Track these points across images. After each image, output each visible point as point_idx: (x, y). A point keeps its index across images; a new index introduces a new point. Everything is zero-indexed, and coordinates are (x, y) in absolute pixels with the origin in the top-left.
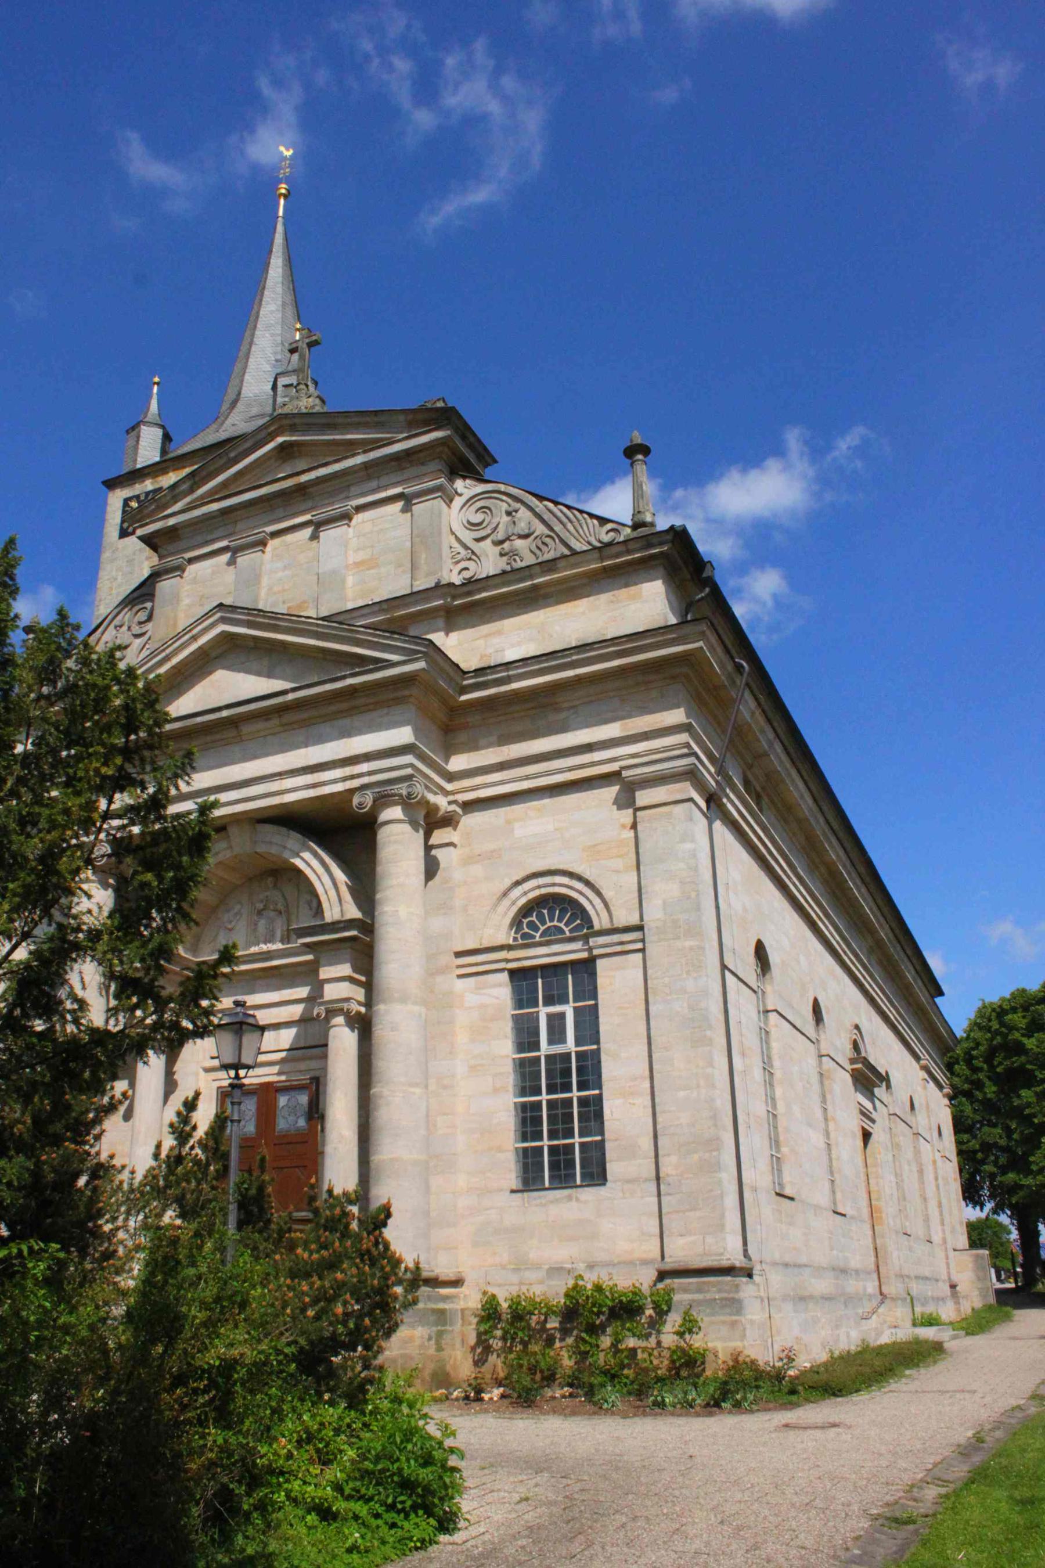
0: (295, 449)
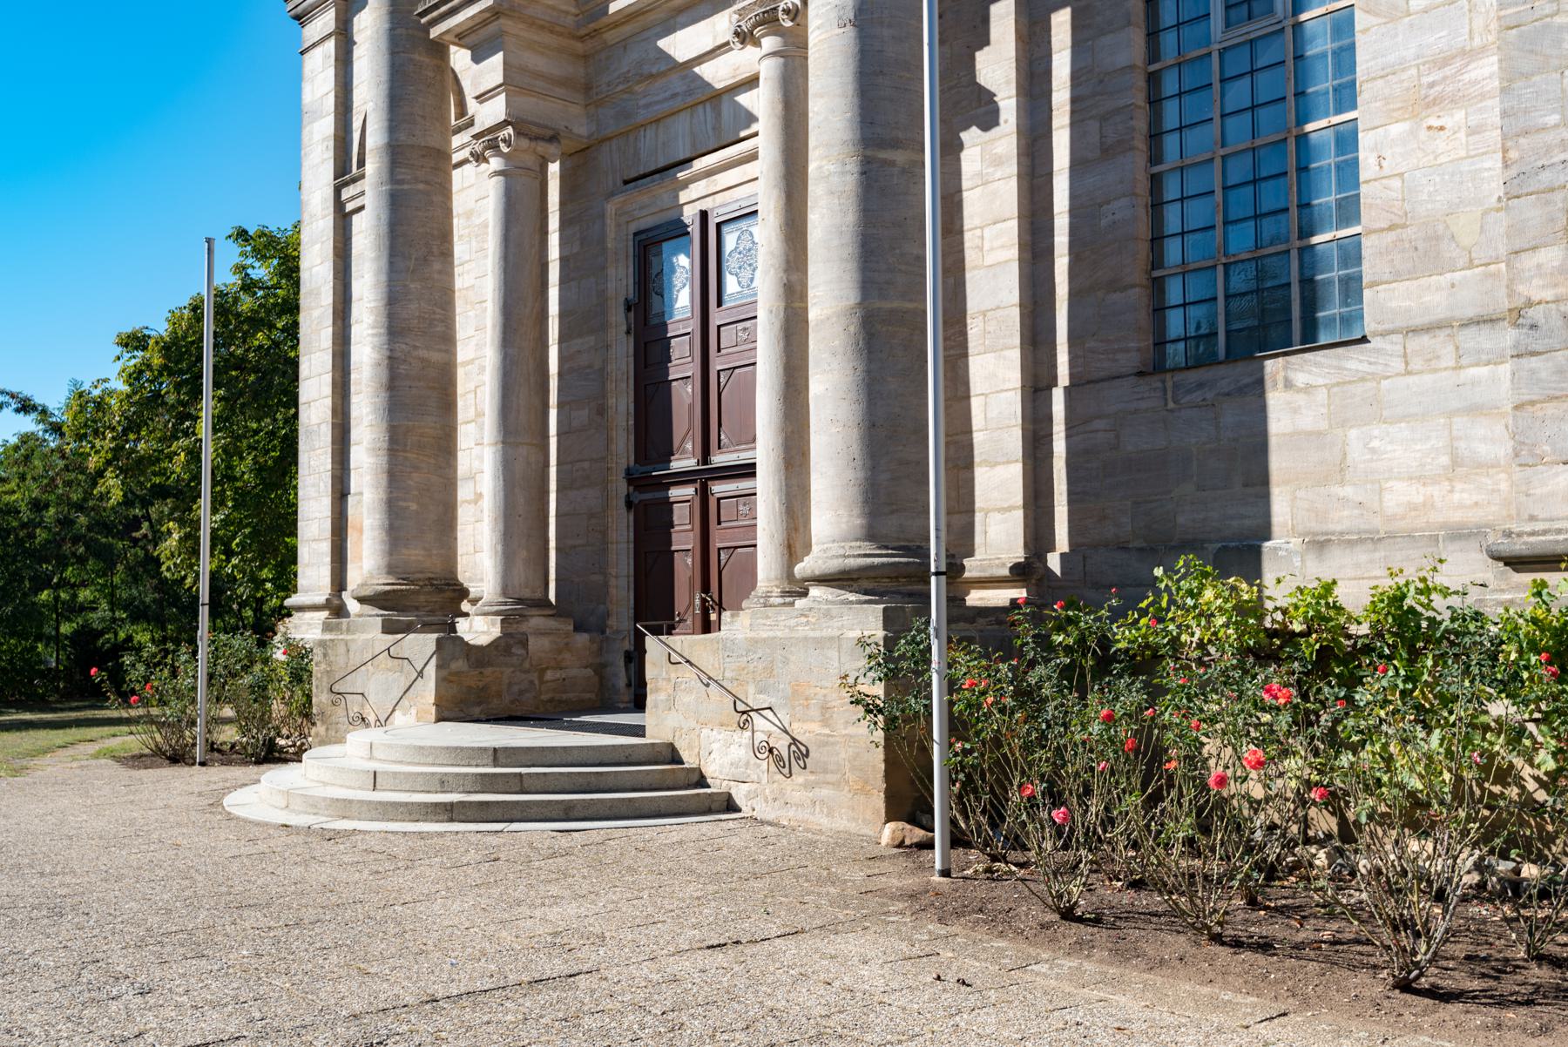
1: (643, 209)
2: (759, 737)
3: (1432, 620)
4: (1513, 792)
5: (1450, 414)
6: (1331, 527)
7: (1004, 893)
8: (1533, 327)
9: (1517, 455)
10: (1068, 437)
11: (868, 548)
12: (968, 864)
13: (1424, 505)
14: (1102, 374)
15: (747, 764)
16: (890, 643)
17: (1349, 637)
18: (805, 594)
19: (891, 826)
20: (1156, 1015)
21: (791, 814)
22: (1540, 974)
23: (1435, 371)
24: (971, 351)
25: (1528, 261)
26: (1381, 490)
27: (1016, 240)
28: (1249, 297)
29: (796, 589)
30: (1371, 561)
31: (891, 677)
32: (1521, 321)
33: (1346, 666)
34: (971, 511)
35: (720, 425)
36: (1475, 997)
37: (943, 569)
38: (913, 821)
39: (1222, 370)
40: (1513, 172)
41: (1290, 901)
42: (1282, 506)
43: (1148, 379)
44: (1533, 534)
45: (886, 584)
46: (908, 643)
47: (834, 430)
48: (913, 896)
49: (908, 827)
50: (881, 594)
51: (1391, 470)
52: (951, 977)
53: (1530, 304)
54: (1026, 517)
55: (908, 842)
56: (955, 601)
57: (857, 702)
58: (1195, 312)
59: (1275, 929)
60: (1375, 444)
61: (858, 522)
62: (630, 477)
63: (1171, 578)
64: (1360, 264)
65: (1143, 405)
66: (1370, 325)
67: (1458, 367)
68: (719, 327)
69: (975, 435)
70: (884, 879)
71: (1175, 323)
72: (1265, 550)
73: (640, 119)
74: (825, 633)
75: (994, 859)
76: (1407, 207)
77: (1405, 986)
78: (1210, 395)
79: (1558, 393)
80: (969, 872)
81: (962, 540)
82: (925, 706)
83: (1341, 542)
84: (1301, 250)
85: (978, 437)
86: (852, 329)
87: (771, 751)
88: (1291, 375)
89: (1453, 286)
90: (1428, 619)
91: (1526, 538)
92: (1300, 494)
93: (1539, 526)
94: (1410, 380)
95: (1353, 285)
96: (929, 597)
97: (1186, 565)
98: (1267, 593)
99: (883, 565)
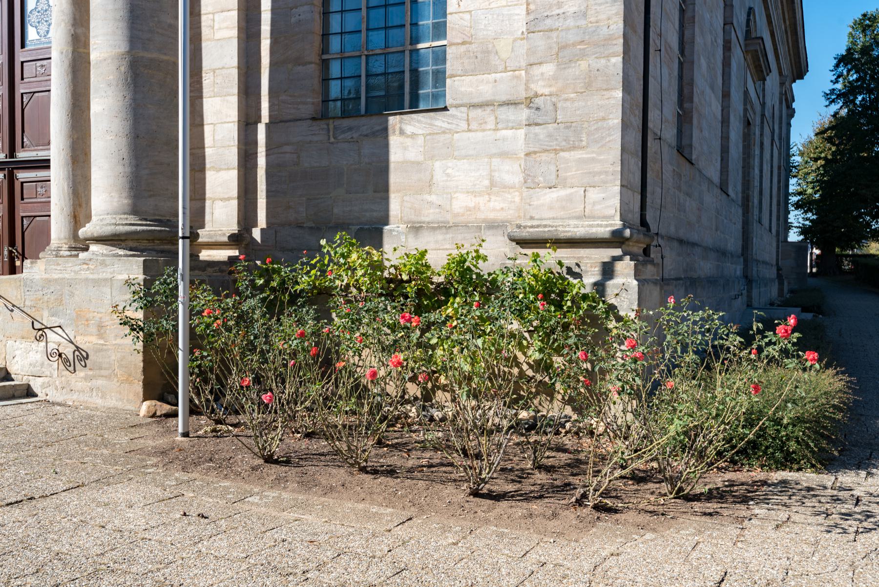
2: (51, 346)
3: (478, 275)
4: (515, 371)
5: (491, 156)
6: (423, 219)
7: (225, 444)
8: (538, 109)
9: (525, 182)
10: (267, 155)
11: (132, 219)
12: (200, 427)
13: (474, 208)
14: (290, 117)
15: (42, 365)
16: (148, 284)
17: (432, 283)
18: (86, 249)
19: (147, 404)
20: (333, 527)
21: (75, 397)
22: (541, 477)
23: (484, 130)
24: (204, 95)
25: (537, 71)
26: (452, 198)
27: (236, 25)
28: (380, 77)
29: (80, 245)
30: (444, 239)
31: (149, 306)
32: (531, 105)
33: (430, 301)
34: (203, 199)
35: (23, 131)
36: (513, 496)
37: (188, 235)
38: (162, 399)
39: (364, 120)
40: (532, 17)
41: (400, 440)
42: (398, 205)
43: (318, 122)
44: (532, 227)
45: (144, 244)
46: (161, 284)
47: (109, 138)
48: (163, 453)
49: (159, 403)
50: (142, 251)
51: (457, 187)
52: (193, 512)
53: (536, 95)
54: (239, 205)
55: (158, 413)
56: (194, 257)
57: (125, 323)
58: (349, 83)
59: (395, 459)
60: (449, 171)
61: (126, 201)
63: (330, 246)
64: (445, 64)
65: (315, 138)
66: (449, 101)
67: (496, 130)
68: (22, 63)
69: (207, 150)
70: (142, 441)
71: (335, 89)
72: (385, 231)
74: (101, 276)
75: (218, 422)
76: (473, 32)
77: (476, 494)
78: (355, 135)
79: (548, 148)
80: (201, 432)
81: (198, 218)
82: (173, 325)
83: (428, 228)
84: (411, 51)
85: (208, 152)
86: (123, 69)
87: (60, 355)
88: (404, 127)
89: (495, 81)
90: (476, 273)
91: (528, 229)
92: (406, 198)
93: (535, 223)
94: (470, 134)
95: (440, 76)
96: (178, 254)
97: (341, 238)
98: (385, 256)
99: (143, 231)
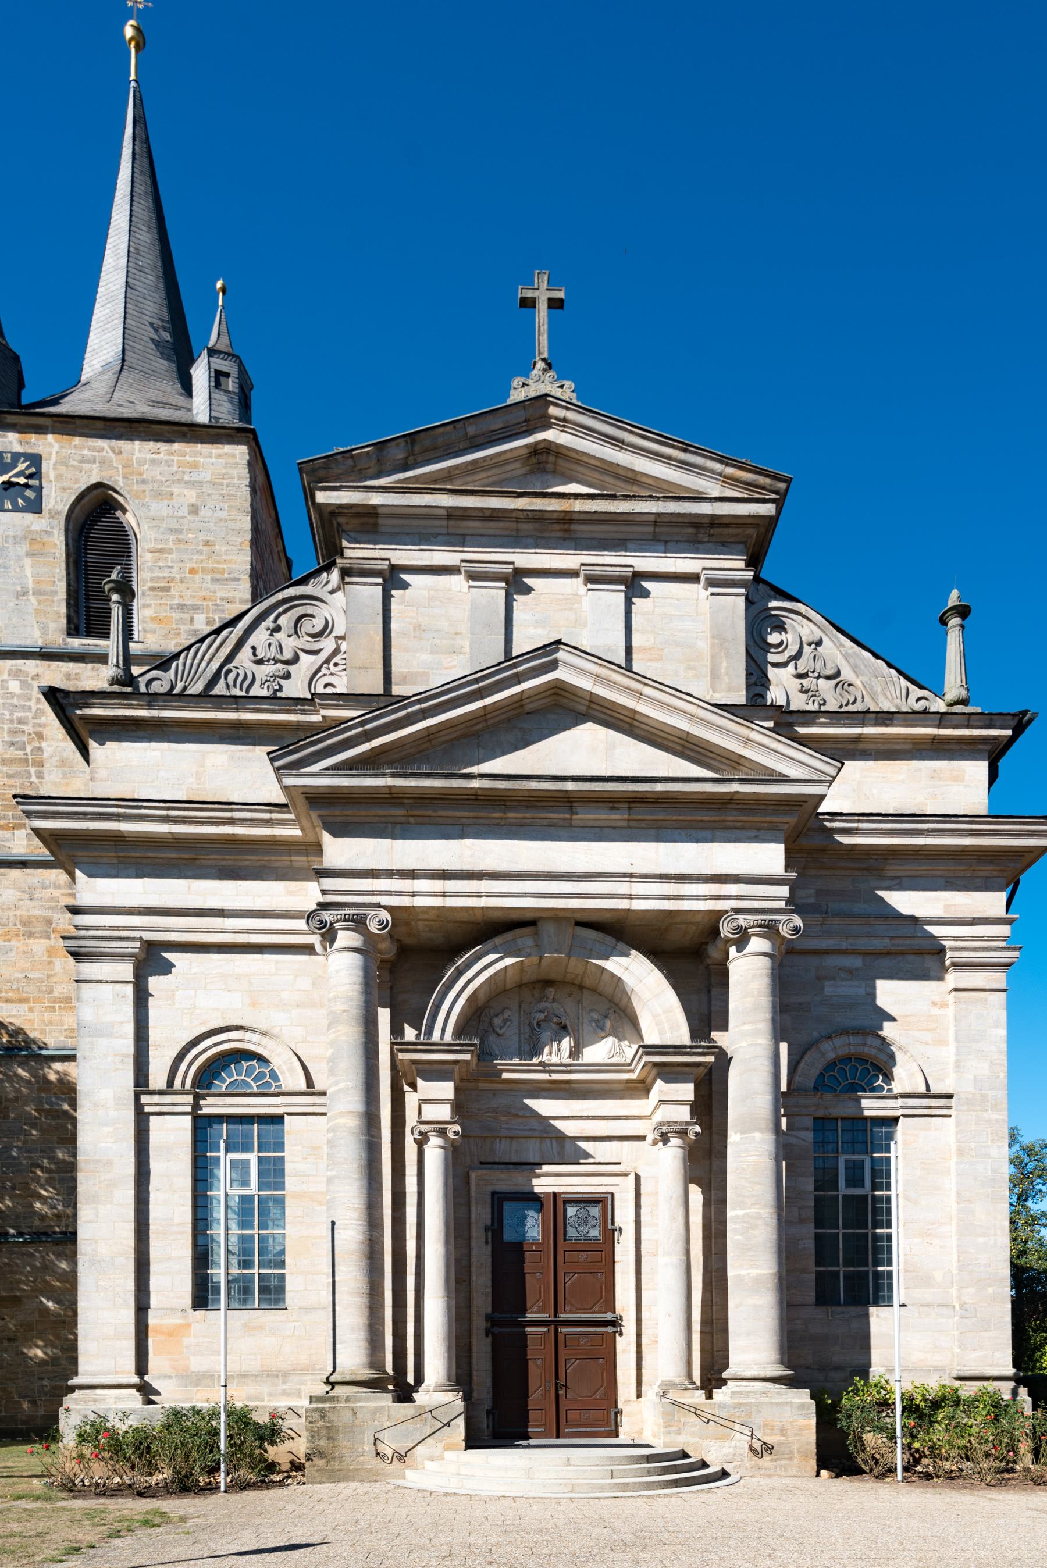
0: (551, 459)
1: (506, 1181)
62: (488, 1318)
73: (501, 1134)
